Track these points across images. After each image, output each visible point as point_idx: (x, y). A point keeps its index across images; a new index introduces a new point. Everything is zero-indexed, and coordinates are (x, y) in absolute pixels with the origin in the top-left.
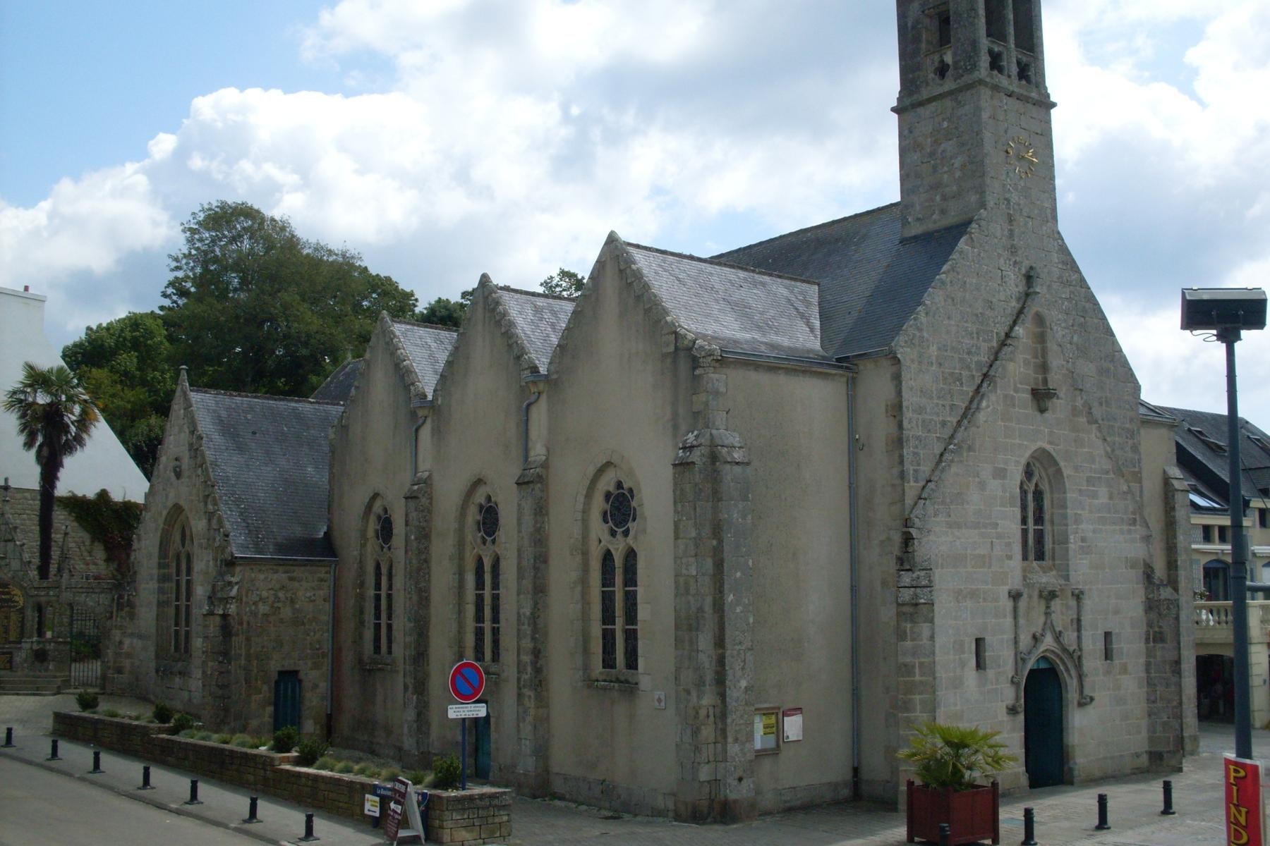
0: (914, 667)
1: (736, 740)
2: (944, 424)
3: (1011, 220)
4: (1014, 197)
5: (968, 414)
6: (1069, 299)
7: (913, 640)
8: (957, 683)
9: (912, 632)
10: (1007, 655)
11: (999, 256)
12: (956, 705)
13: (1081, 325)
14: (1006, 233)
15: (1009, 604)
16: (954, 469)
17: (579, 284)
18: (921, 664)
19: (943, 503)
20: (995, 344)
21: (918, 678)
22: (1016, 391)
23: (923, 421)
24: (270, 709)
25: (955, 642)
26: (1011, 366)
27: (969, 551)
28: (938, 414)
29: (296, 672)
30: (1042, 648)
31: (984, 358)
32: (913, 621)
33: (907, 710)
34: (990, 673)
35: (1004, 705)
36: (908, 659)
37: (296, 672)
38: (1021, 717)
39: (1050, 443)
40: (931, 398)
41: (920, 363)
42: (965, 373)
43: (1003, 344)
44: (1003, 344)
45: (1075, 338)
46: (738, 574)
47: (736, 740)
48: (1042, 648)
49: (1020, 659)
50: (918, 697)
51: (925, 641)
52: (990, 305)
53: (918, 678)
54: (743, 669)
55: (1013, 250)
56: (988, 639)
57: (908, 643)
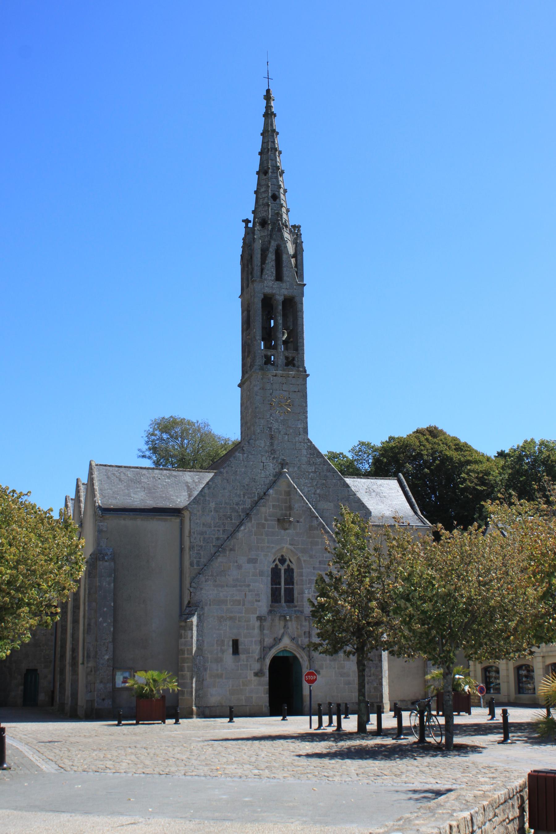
0: (185, 651)
1: (101, 682)
2: (218, 539)
3: (272, 437)
4: (275, 426)
5: (232, 535)
6: (315, 472)
7: (184, 638)
8: (219, 660)
9: (185, 635)
10: (256, 649)
11: (262, 456)
12: (217, 670)
13: (323, 484)
14: (268, 444)
15: (257, 624)
16: (220, 560)
17: (218, 459)
18: (188, 649)
19: (212, 575)
20: (256, 498)
21: (186, 656)
22: (266, 520)
23: (204, 538)
24: (22, 687)
25: (217, 641)
26: (263, 509)
27: (229, 598)
28: (214, 535)
29: (37, 670)
30: (281, 646)
31: (248, 506)
32: (185, 630)
33: (182, 671)
34: (242, 656)
35: (253, 672)
36: (183, 647)
37: (37, 670)
38: (266, 679)
39: (291, 544)
40: (210, 527)
41: (203, 511)
42: (234, 515)
43: (261, 498)
44: (261, 498)
45: (318, 491)
46: (105, 609)
47: (101, 682)
48: (281, 646)
49: (265, 650)
50: (186, 665)
51: (189, 639)
52: (254, 480)
53: (186, 656)
54: (106, 650)
55: (273, 451)
56: (241, 640)
57: (183, 640)
